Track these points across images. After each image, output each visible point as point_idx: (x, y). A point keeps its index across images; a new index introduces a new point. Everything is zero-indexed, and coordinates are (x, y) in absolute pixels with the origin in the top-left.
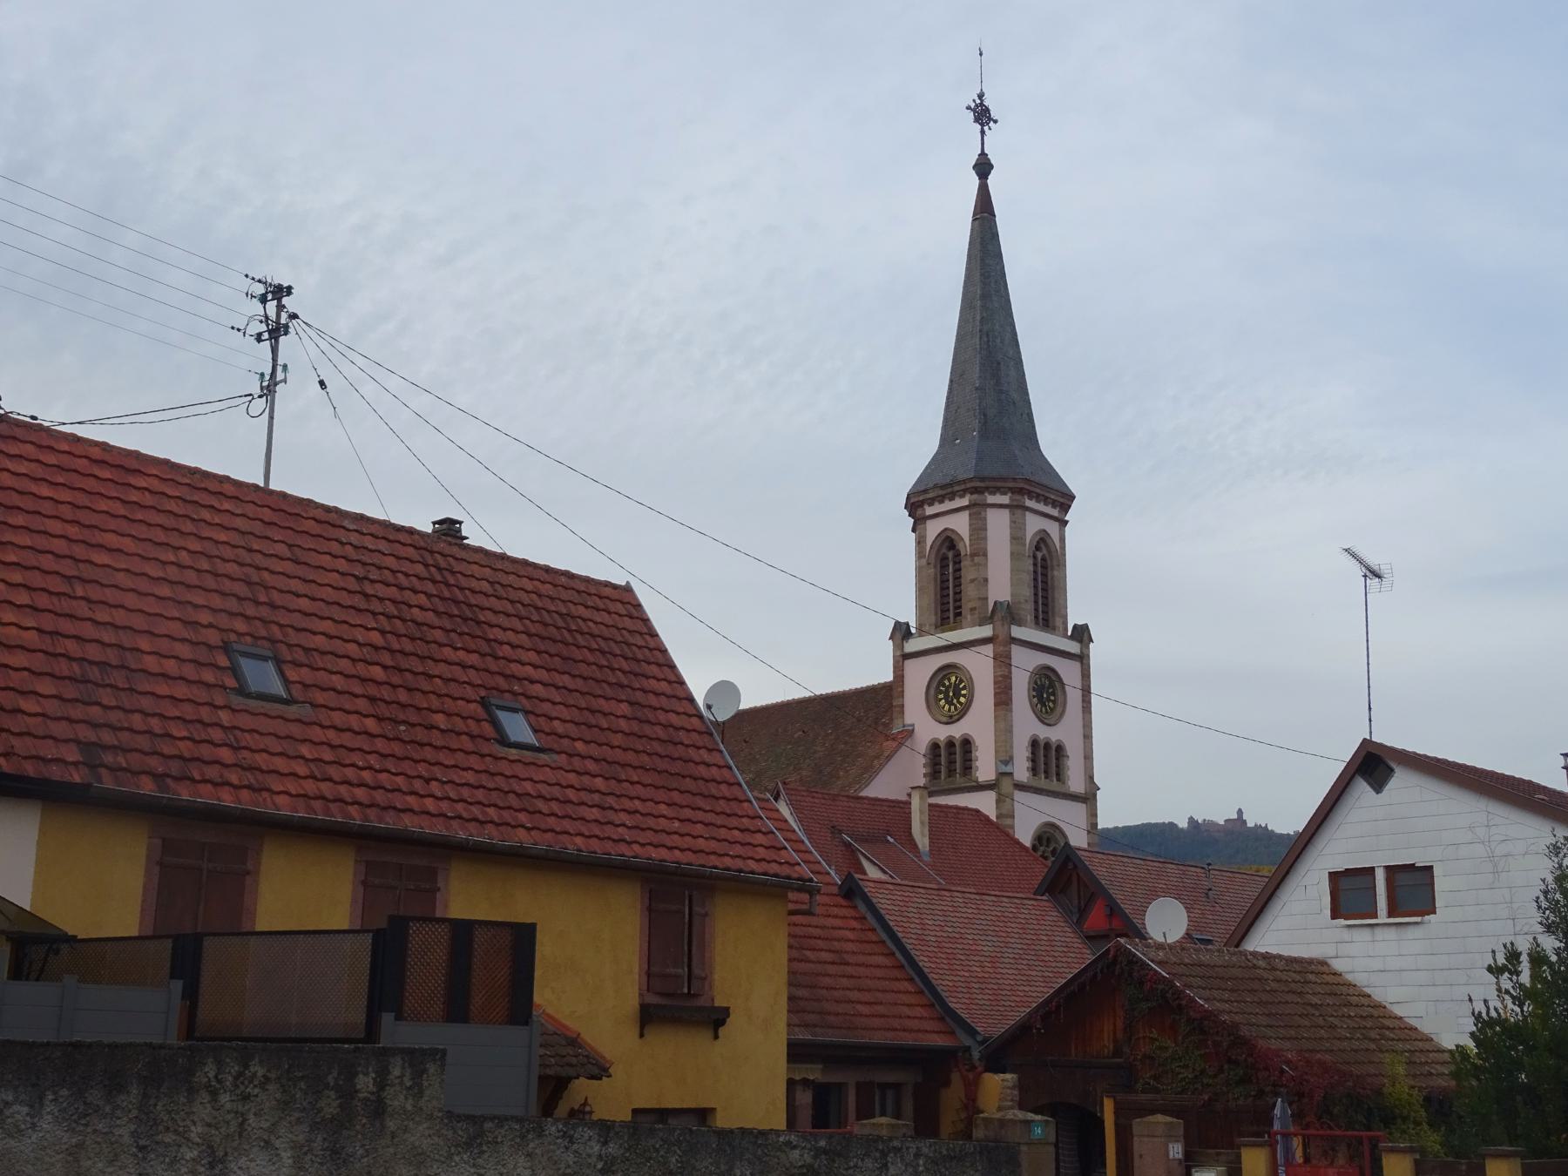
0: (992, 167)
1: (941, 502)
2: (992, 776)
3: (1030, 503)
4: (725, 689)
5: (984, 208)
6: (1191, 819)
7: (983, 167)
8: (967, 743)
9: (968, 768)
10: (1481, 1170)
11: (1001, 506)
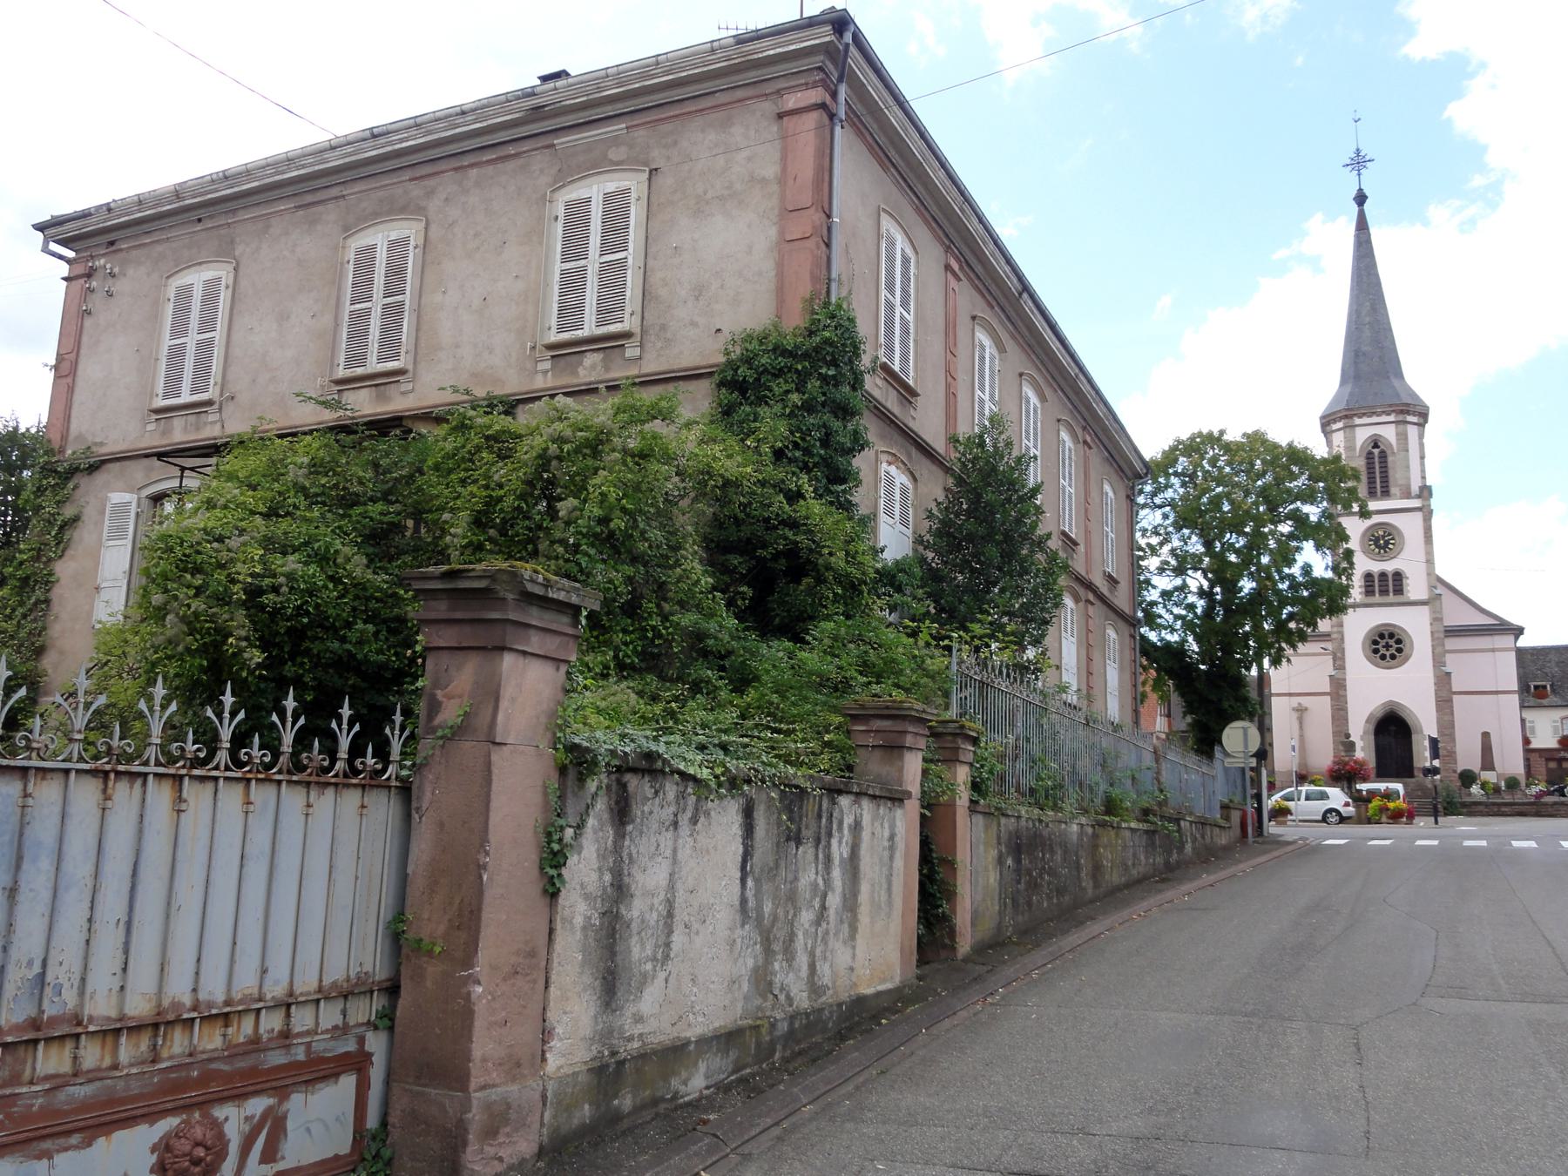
2: (1424, 596)
3: (1358, 421)
5: (1362, 225)
7: (1361, 199)
8: (1398, 576)
9: (1399, 590)
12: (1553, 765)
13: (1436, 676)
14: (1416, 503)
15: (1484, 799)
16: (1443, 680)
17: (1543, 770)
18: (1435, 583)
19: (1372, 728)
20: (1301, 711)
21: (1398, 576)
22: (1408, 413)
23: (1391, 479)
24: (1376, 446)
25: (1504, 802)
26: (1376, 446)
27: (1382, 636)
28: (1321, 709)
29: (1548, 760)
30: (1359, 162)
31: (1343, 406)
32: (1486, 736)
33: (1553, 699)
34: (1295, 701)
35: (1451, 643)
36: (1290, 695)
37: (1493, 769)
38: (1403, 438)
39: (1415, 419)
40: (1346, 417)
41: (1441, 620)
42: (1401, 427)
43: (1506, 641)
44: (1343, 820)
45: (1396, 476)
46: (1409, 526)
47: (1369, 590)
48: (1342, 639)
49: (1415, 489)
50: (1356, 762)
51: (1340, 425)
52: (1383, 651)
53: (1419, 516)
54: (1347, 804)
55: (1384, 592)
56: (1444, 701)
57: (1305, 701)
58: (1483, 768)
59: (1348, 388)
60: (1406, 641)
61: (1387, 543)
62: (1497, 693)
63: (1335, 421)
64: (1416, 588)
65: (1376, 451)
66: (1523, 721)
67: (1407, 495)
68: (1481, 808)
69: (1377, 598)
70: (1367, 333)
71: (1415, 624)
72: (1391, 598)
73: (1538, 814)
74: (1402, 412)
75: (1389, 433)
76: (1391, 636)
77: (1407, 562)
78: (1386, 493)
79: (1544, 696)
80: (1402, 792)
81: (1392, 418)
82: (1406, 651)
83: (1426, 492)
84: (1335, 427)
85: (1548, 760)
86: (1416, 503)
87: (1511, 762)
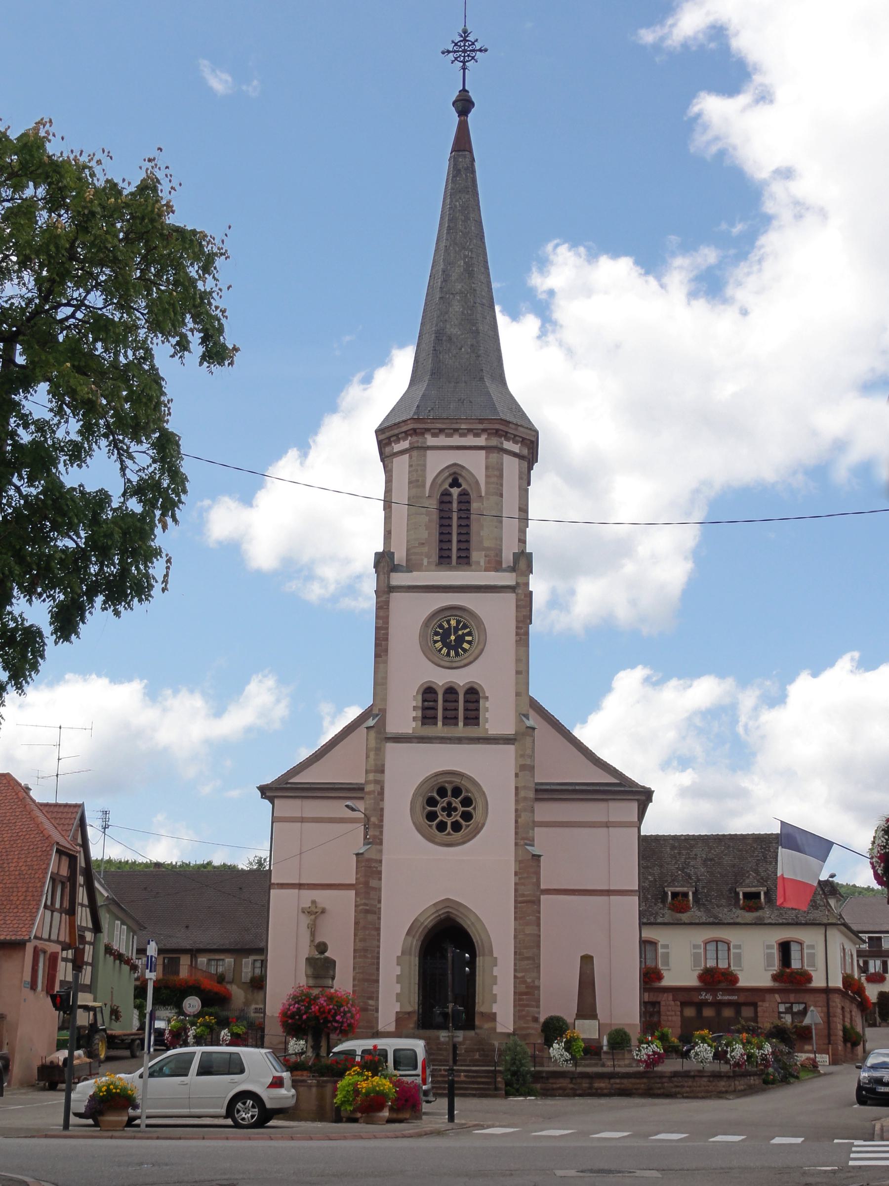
0: (472, 104)
1: (449, 435)
2: (509, 729)
3: (431, 441)
4: (487, 710)
5: (462, 144)
6: (71, 642)
7: (464, 105)
8: (473, 694)
9: (473, 719)
10: (886, 951)
11: (515, 455)
12: (690, 1012)
13: (519, 861)
14: (508, 579)
15: (570, 1067)
16: (529, 866)
17: (677, 1020)
18: (525, 708)
19: (415, 944)
20: (315, 913)
21: (473, 694)
22: (506, 436)
23: (474, 539)
24: (455, 483)
25: (600, 1074)
26: (455, 483)
27: (442, 792)
28: (342, 907)
29: (684, 1004)
30: (465, 50)
31: (410, 414)
32: (587, 961)
33: (695, 913)
34: (307, 896)
35: (546, 811)
36: (300, 886)
37: (594, 1016)
38: (496, 473)
39: (516, 448)
40: (415, 432)
41: (531, 768)
42: (494, 456)
43: (627, 810)
44: (266, 1116)
45: (482, 533)
46: (494, 613)
47: (427, 716)
48: (381, 793)
49: (507, 558)
50: (330, 998)
51: (405, 445)
52: (442, 817)
53: (511, 597)
54: (277, 1083)
55: (450, 719)
56: (527, 905)
57: (321, 896)
58: (581, 1015)
59: (422, 388)
60: (479, 802)
61: (460, 640)
62: (608, 893)
63: (398, 438)
64: (498, 717)
65: (455, 491)
66: (645, 944)
67: (496, 565)
68: (564, 1083)
69: (440, 729)
70: (457, 307)
71: (490, 771)
72: (461, 729)
73: (649, 1093)
74: (497, 433)
75: (475, 464)
76: (457, 791)
77: (486, 672)
78: (465, 560)
79: (684, 909)
80: (421, 1055)
81: (481, 441)
82: (477, 816)
83: (523, 562)
84: (397, 447)
85: (684, 1004)
86: (508, 579)
87: (621, 1005)
